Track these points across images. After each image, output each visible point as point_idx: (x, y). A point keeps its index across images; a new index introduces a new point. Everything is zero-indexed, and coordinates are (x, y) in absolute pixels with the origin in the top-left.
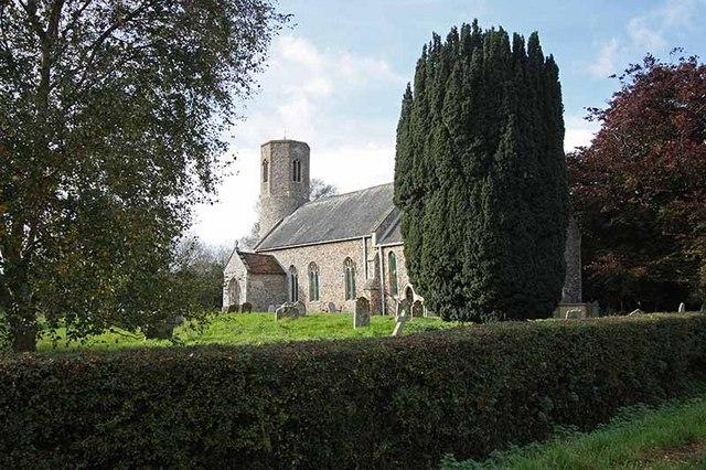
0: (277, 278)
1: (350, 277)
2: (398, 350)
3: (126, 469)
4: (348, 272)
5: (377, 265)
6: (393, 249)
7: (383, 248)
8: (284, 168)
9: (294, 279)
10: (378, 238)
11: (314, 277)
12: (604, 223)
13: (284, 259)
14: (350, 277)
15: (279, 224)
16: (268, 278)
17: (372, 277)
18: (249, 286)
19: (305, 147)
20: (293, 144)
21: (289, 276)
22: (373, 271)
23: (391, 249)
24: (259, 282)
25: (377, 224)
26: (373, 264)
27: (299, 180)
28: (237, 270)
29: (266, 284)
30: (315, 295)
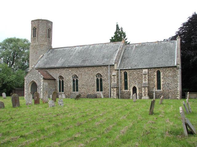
0: (52, 82)
7: (121, 70)
8: (42, 32)
11: (76, 83)
16: (49, 81)
19: (51, 23)
26: (116, 77)
27: (50, 38)
29: (49, 84)
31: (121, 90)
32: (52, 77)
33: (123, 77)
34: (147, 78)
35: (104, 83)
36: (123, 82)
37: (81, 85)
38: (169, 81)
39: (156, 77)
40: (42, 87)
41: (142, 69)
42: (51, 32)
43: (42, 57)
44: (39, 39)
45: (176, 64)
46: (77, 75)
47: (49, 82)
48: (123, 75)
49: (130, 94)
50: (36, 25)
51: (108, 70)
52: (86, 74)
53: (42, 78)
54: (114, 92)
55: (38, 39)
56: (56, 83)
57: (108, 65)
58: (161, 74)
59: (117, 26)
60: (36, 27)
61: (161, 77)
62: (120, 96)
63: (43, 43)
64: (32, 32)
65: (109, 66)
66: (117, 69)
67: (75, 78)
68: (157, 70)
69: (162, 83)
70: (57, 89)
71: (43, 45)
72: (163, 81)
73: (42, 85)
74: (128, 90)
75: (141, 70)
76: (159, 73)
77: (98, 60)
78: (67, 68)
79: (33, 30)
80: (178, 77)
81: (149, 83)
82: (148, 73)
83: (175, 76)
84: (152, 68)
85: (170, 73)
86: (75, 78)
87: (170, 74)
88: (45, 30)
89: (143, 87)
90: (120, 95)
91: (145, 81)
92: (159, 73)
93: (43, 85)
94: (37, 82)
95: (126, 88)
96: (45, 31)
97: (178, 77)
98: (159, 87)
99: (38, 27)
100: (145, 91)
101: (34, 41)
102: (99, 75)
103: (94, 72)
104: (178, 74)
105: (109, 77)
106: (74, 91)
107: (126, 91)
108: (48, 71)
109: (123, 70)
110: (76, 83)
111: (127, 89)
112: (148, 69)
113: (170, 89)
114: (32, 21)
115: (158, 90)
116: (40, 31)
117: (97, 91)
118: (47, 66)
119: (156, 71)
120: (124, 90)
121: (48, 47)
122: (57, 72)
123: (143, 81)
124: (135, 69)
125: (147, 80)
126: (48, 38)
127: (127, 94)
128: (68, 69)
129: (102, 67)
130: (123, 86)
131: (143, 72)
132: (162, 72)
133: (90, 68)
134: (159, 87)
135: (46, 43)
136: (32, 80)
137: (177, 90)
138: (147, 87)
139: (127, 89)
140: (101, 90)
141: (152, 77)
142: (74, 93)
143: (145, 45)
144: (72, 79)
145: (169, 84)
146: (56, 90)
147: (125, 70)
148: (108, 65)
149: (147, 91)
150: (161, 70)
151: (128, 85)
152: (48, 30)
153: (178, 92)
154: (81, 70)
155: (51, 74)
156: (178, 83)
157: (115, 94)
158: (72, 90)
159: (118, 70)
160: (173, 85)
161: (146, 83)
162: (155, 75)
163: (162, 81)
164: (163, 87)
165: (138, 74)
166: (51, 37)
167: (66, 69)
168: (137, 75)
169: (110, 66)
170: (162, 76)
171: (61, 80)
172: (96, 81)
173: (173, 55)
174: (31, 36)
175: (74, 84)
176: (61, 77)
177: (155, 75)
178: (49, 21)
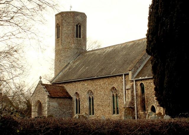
0: (67, 101)
1: (115, 97)
2: (126, 125)
4: (113, 97)
5: (132, 92)
6: (143, 82)
7: (136, 81)
8: (69, 30)
9: (78, 102)
10: (133, 74)
11: (91, 100)
12: (146, 119)
13: (71, 89)
14: (115, 97)
15: (67, 66)
16: (61, 101)
19: (83, 16)
20: (75, 14)
21: (74, 98)
22: (130, 96)
23: (141, 82)
24: (55, 104)
25: (132, 65)
26: (130, 91)
27: (80, 37)
28: (45, 98)
29: (60, 104)
30: (91, 110)
35: (119, 100)
40: (46, 108)
42: (82, 29)
44: (63, 41)
46: (93, 91)
47: (61, 102)
48: (139, 88)
53: (47, 97)
56: (71, 104)
57: (121, 75)
64: (56, 31)
71: (68, 48)
73: (46, 105)
88: (71, 26)
93: (49, 105)
108: (65, 86)
116: (64, 29)
117: (90, 115)
121: (76, 51)
126: (77, 37)
128: (84, 83)
129: (118, 77)
135: (73, 45)
136: (38, 99)
147: (141, 80)
150: (126, 88)
152: (77, 26)
169: (125, 75)
172: (111, 98)
175: (90, 104)
178: (77, 13)
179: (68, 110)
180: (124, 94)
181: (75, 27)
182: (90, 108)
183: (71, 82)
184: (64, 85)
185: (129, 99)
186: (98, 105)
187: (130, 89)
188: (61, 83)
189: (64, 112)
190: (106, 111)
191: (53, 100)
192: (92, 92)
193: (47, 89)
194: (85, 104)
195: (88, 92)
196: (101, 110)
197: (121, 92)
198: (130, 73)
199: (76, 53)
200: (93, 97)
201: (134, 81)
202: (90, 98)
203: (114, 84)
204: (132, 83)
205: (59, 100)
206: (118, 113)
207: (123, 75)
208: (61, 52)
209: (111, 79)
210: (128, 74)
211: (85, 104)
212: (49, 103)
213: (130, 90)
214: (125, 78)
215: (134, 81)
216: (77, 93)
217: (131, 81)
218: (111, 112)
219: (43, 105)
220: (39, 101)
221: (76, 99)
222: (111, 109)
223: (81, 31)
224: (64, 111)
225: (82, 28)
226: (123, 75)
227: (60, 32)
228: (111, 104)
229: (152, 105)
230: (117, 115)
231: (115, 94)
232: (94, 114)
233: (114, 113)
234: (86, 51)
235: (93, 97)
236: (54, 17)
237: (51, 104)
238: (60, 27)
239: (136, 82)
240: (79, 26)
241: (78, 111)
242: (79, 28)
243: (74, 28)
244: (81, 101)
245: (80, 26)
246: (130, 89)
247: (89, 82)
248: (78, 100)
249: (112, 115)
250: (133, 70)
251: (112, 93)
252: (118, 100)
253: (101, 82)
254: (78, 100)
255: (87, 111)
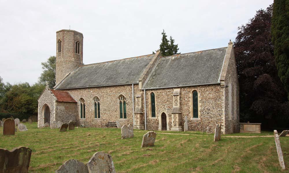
0: (72, 106)
1: (123, 104)
3: (56, 172)
5: (142, 100)
6: (154, 92)
7: (146, 90)
8: (69, 45)
9: (83, 107)
10: (143, 84)
11: (97, 106)
13: (76, 96)
16: (68, 105)
17: (140, 107)
18: (57, 109)
19: (81, 35)
20: (76, 33)
21: (79, 103)
22: (140, 104)
23: (151, 92)
24: (62, 107)
26: (140, 99)
27: (79, 53)
29: (65, 107)
30: (97, 114)
31: (147, 117)
32: (72, 99)
33: (149, 100)
34: (179, 101)
35: (127, 107)
36: (150, 106)
37: (103, 110)
38: (210, 105)
39: (191, 100)
40: (54, 112)
41: (172, 88)
42: (80, 46)
43: (68, 75)
44: (64, 54)
45: (219, 82)
46: (98, 97)
48: (149, 97)
49: (158, 123)
50: (61, 38)
51: (132, 90)
52: (108, 96)
53: (55, 101)
54: (138, 120)
55: (63, 53)
56: (76, 108)
57: (132, 84)
58: (199, 95)
59: (164, 37)
60: (61, 40)
61: (199, 99)
62: (146, 125)
63: (69, 59)
65: (133, 86)
66: (143, 89)
67: (122, 100)
68: (193, 90)
69: (199, 108)
70: (79, 115)
71: (69, 61)
72: (201, 106)
73: (54, 109)
74: (156, 118)
75: (171, 90)
76: (195, 94)
77: (122, 78)
78: (89, 88)
79: (58, 44)
80: (222, 100)
81: (181, 109)
82: (181, 94)
83: (217, 98)
84: (186, 87)
85: (211, 94)
86: (122, 100)
87: (211, 96)
89: (172, 113)
90: (146, 123)
91: (176, 105)
92: (195, 94)
94: (50, 106)
95: (154, 115)
96: (71, 44)
97: (222, 100)
98: (195, 115)
99: (63, 39)
100: (175, 120)
101: (60, 57)
102: (96, 98)
103: (115, 92)
104: (223, 96)
105: (133, 100)
106: (96, 117)
107: (154, 119)
108: (69, 92)
109: (149, 90)
110: (97, 106)
111: (155, 116)
112: (181, 89)
113: (211, 118)
114: (57, 32)
115: (195, 119)
116: (66, 44)
118: (68, 87)
119: (191, 92)
120: (150, 117)
122: (78, 93)
123: (174, 105)
124: (164, 89)
125: (179, 104)
126: (76, 52)
127: (154, 122)
128: (89, 90)
129: (126, 87)
130: (150, 113)
131: (174, 92)
132: (199, 92)
133: (112, 89)
134: (195, 115)
137: (221, 120)
138: (177, 113)
139: (155, 116)
140: (125, 117)
141: (186, 99)
142: (96, 120)
143: (184, 57)
144: (93, 102)
145: (209, 110)
146: (78, 115)
147: (152, 90)
148: (132, 84)
149: (177, 120)
150: (198, 90)
151: (156, 111)
153: (222, 123)
154: (104, 90)
155: (72, 96)
156: (222, 110)
157: (139, 122)
158: (93, 116)
159: (143, 90)
160: (215, 112)
161: (176, 109)
162: (189, 98)
163: (200, 106)
164: (201, 115)
165: (168, 95)
166: (80, 52)
167: (87, 90)
168: (166, 97)
169: (134, 85)
170: (200, 98)
171: (83, 104)
172: (119, 104)
173: (218, 68)
174: (57, 51)
175: (96, 109)
176: (82, 99)
177: (189, 98)
179: (73, 113)
180: (133, 102)
181: (75, 44)
182: (96, 112)
183: (103, 87)
184: (68, 92)
185: (139, 106)
186: (105, 110)
187: (140, 97)
188: (65, 90)
189: (70, 115)
190: (113, 115)
191: (61, 104)
192: (98, 98)
193: (54, 94)
194: (90, 109)
195: (94, 98)
196: (107, 114)
197: (129, 100)
198: (140, 83)
199: (75, 65)
200: (84, 104)
201: (144, 90)
202: (95, 103)
203: (122, 92)
204: (142, 92)
205: (65, 104)
206: (125, 117)
207: (133, 84)
208: (63, 64)
209: (118, 88)
210: (138, 84)
211: (90, 109)
212: (57, 107)
213: (140, 98)
214: (134, 88)
215: (144, 90)
216: (82, 99)
217: (141, 90)
218: (119, 116)
219: (51, 108)
220: (46, 104)
221: (81, 103)
222: (118, 113)
223: (80, 49)
224: (70, 113)
225: (80, 46)
226: (133, 84)
227: (61, 47)
228: (118, 110)
229: (163, 112)
230: (125, 119)
231: (122, 101)
232: (101, 117)
233: (121, 117)
234: (83, 65)
235: (84, 104)
236: (55, 35)
237: (59, 107)
238: (62, 43)
239: (146, 92)
240: (78, 43)
241: (83, 115)
242: (78, 46)
243: (74, 44)
244: (87, 105)
245: (79, 44)
246: (140, 97)
247: (96, 90)
248: (83, 105)
249: (119, 119)
250: (143, 81)
251: (119, 100)
252: (126, 106)
253: (108, 90)
254: (83, 105)
255: (92, 115)
